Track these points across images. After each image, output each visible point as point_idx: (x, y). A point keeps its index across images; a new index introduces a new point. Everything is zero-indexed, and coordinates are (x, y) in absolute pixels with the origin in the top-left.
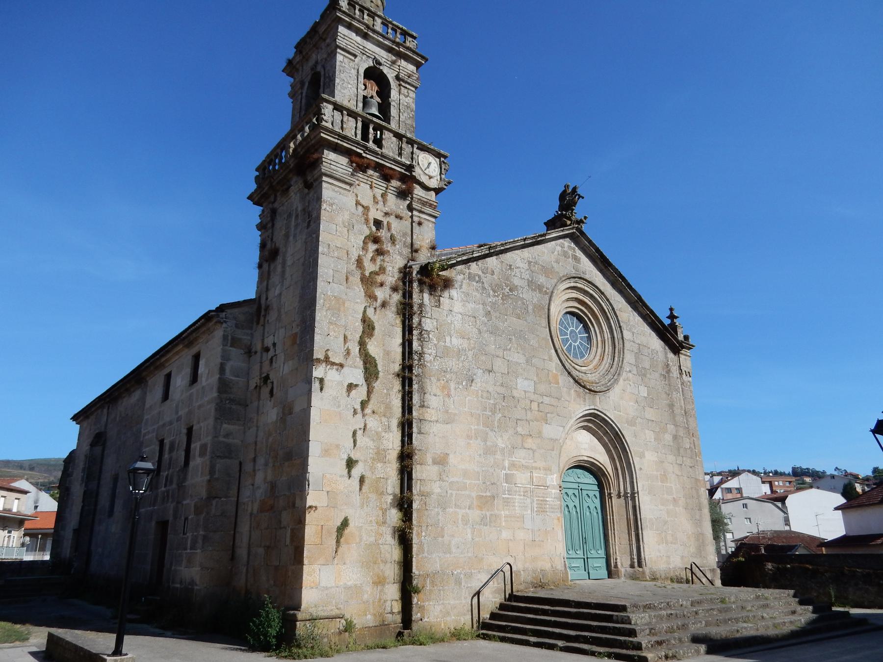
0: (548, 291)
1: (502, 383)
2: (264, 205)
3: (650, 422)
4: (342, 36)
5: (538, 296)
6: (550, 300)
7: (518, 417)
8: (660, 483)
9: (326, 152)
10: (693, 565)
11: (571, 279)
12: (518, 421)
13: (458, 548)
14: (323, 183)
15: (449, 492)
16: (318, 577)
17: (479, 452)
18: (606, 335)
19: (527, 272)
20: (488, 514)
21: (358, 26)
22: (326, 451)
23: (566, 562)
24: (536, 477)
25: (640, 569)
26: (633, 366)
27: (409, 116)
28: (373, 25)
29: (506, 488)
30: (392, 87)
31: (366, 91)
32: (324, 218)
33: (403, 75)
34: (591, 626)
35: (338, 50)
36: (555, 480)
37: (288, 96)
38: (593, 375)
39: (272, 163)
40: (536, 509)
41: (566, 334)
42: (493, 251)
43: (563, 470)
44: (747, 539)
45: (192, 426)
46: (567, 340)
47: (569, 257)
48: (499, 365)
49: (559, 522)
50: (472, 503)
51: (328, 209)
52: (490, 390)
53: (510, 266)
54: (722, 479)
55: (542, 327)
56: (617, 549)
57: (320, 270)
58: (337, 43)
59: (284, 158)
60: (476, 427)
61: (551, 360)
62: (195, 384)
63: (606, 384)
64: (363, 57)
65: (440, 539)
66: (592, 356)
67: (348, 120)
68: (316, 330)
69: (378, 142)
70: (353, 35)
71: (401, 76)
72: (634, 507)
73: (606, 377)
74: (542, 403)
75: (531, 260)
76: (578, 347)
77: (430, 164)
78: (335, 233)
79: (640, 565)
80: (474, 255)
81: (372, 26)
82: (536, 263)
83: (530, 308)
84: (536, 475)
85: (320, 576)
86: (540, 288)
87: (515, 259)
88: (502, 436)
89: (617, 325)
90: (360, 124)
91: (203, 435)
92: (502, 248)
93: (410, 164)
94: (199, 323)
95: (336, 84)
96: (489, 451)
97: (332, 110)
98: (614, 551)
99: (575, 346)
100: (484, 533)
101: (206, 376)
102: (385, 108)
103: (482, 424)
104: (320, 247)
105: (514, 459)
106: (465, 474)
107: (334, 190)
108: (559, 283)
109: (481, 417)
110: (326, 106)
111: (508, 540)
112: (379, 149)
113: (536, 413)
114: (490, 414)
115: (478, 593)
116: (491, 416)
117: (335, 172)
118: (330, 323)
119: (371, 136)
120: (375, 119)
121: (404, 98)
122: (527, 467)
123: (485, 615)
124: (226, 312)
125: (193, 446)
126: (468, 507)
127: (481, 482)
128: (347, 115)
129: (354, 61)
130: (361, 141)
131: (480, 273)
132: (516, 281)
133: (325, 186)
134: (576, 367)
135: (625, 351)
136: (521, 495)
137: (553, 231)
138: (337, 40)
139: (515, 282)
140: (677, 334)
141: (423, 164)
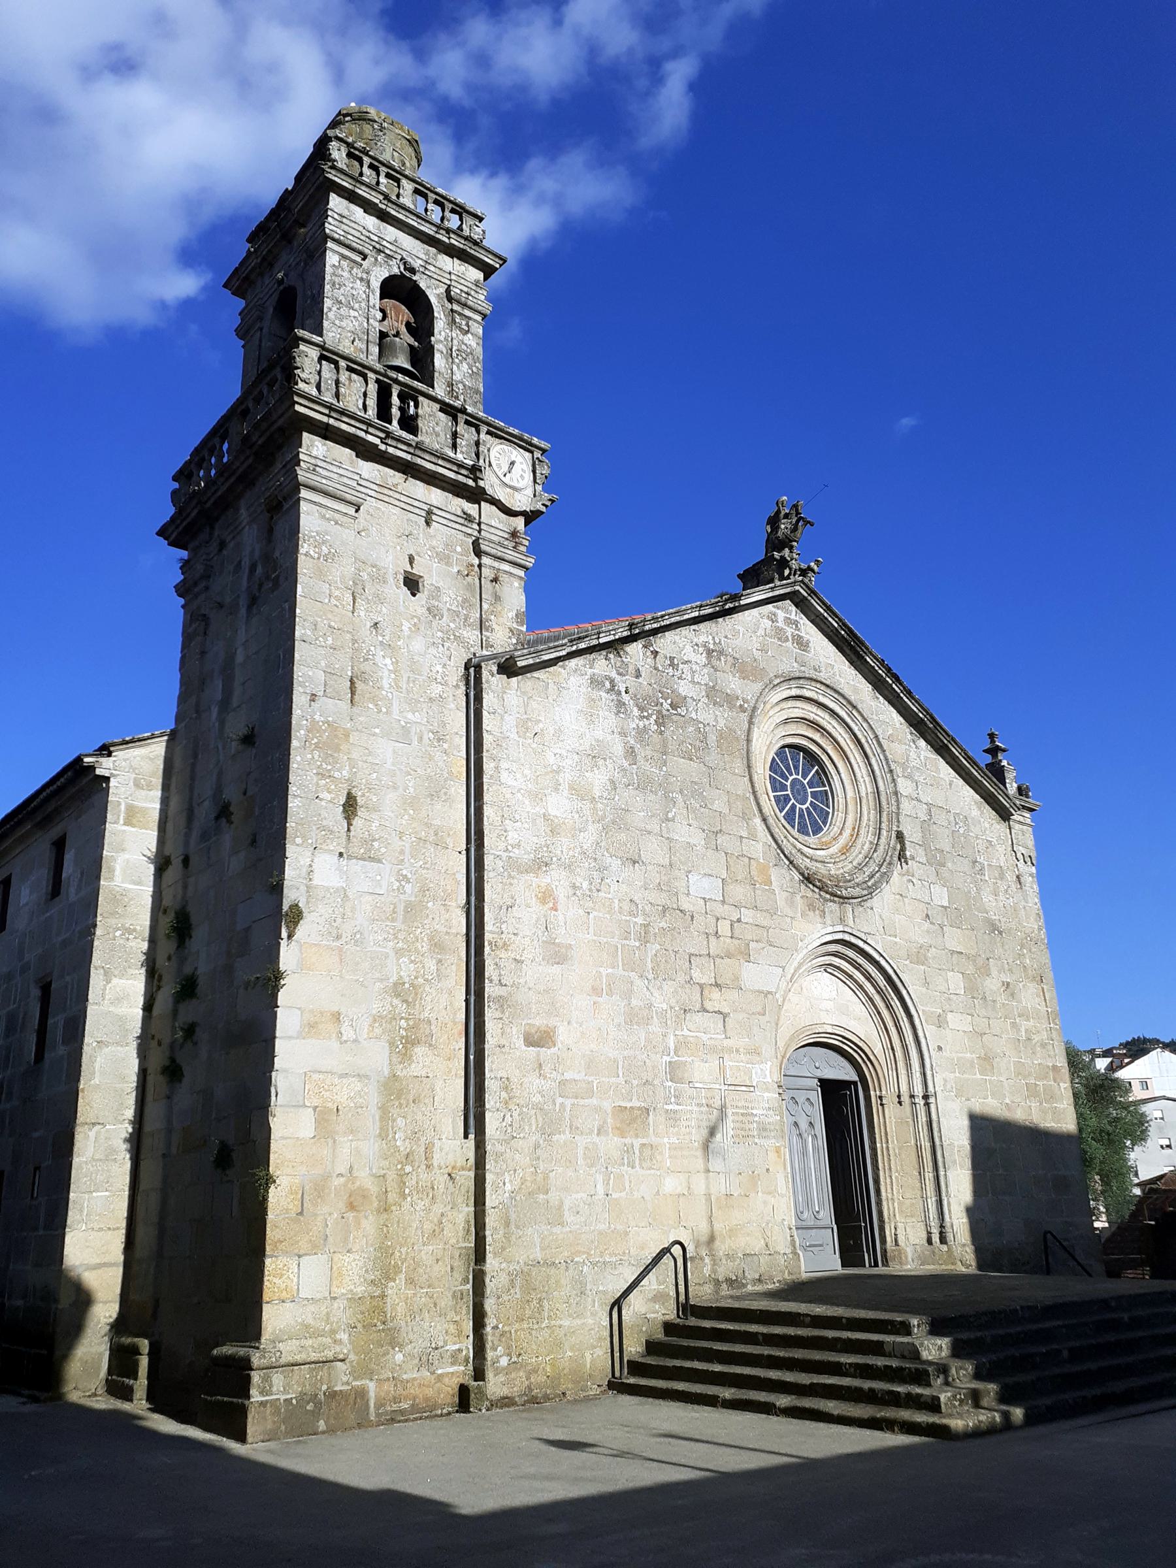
0: (746, 705)
1: (659, 883)
2: (191, 546)
3: (955, 956)
4: (336, 216)
5: (726, 716)
6: (751, 723)
7: (692, 951)
8: (978, 1076)
9: (305, 434)
10: (1049, 1236)
11: (791, 682)
12: (693, 958)
13: (578, 1213)
14: (302, 503)
15: (559, 1100)
16: (295, 1280)
17: (615, 1021)
18: (864, 788)
19: (706, 671)
20: (637, 1143)
21: (368, 196)
22: (312, 1026)
23: (796, 1236)
24: (731, 1068)
25: (944, 1248)
26: (917, 847)
27: (470, 372)
28: (398, 196)
29: (672, 1091)
30: (436, 314)
31: (386, 323)
32: (305, 571)
33: (459, 292)
34: (839, 1364)
35: (330, 244)
36: (768, 1073)
37: (235, 333)
38: (840, 865)
39: (205, 465)
40: (732, 1133)
41: (784, 788)
42: (637, 631)
43: (785, 1054)
44: (1162, 1181)
45: (50, 983)
46: (787, 799)
47: (787, 640)
48: (653, 851)
49: (779, 1157)
50: (605, 1122)
51: (312, 553)
52: (635, 898)
53: (672, 659)
54: (1112, 1062)
55: (734, 774)
56: (897, 1209)
57: (299, 672)
58: (327, 231)
59: (226, 455)
60: (610, 970)
61: (753, 837)
62: (57, 899)
63: (865, 882)
64: (379, 257)
65: (541, 1196)
66: (836, 829)
67: (350, 379)
68: (292, 789)
69: (409, 424)
70: (358, 212)
71: (455, 291)
72: (930, 1123)
73: (865, 869)
74: (739, 921)
75: (712, 647)
76: (807, 812)
77: (513, 463)
78: (327, 601)
79: (943, 1240)
80: (602, 641)
81: (394, 197)
82: (721, 652)
83: (712, 738)
84: (731, 1064)
85: (299, 1277)
86: (730, 700)
87: (681, 646)
88: (660, 988)
89: (885, 767)
90: (373, 388)
91: (71, 1000)
92: (655, 626)
93: (474, 465)
94: (62, 780)
95: (325, 311)
96: (634, 1018)
97: (316, 359)
98: (891, 1212)
99: (801, 810)
100: (630, 1182)
101: (76, 884)
102: (422, 359)
103: (620, 964)
104: (297, 627)
105: (686, 1033)
106: (590, 1064)
107: (323, 517)
108: (767, 690)
109: (620, 950)
110: (303, 352)
111: (679, 1196)
112: (411, 436)
113: (729, 940)
114: (637, 944)
115: (618, 1304)
116: (638, 948)
117: (324, 481)
118: (320, 775)
119: (395, 412)
120: (401, 377)
121: (461, 337)
122: (713, 1050)
123: (634, 1348)
124: (115, 756)
125: (50, 1021)
126: (596, 1132)
127: (621, 1080)
128: (347, 370)
129: (361, 265)
130: (376, 421)
131: (614, 674)
132: (684, 688)
133: (305, 509)
134: (805, 850)
135: (902, 818)
136: (702, 1105)
137: (753, 590)
138: (326, 225)
139: (681, 690)
140: (1004, 785)
141: (499, 466)
